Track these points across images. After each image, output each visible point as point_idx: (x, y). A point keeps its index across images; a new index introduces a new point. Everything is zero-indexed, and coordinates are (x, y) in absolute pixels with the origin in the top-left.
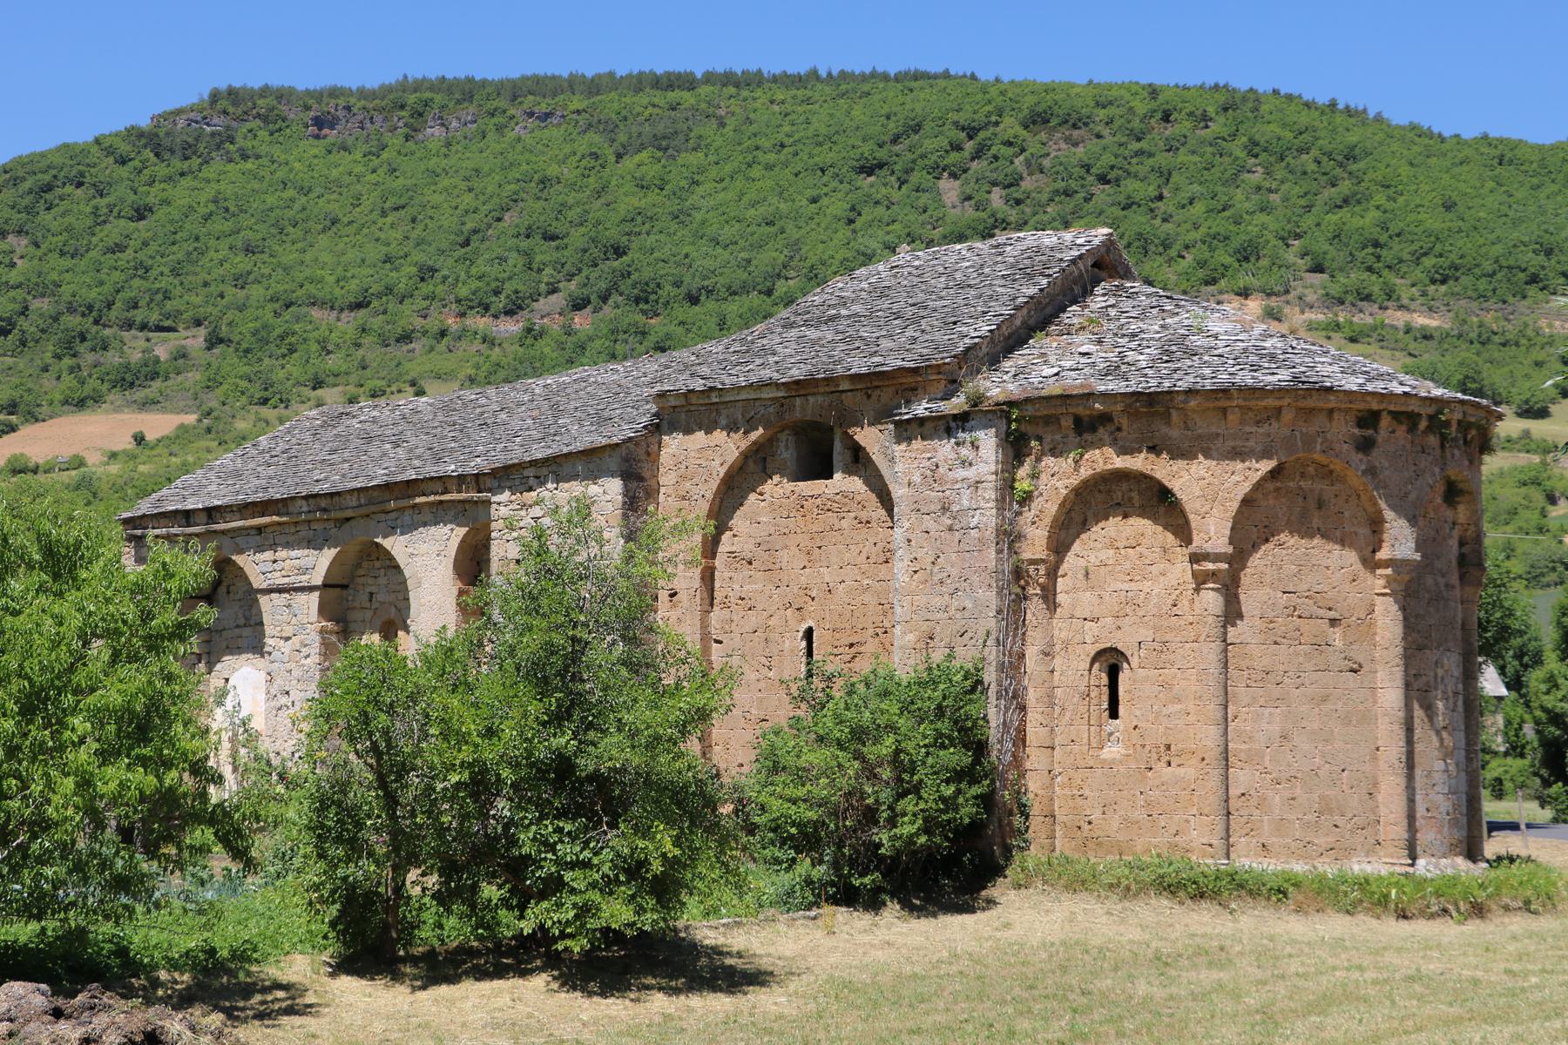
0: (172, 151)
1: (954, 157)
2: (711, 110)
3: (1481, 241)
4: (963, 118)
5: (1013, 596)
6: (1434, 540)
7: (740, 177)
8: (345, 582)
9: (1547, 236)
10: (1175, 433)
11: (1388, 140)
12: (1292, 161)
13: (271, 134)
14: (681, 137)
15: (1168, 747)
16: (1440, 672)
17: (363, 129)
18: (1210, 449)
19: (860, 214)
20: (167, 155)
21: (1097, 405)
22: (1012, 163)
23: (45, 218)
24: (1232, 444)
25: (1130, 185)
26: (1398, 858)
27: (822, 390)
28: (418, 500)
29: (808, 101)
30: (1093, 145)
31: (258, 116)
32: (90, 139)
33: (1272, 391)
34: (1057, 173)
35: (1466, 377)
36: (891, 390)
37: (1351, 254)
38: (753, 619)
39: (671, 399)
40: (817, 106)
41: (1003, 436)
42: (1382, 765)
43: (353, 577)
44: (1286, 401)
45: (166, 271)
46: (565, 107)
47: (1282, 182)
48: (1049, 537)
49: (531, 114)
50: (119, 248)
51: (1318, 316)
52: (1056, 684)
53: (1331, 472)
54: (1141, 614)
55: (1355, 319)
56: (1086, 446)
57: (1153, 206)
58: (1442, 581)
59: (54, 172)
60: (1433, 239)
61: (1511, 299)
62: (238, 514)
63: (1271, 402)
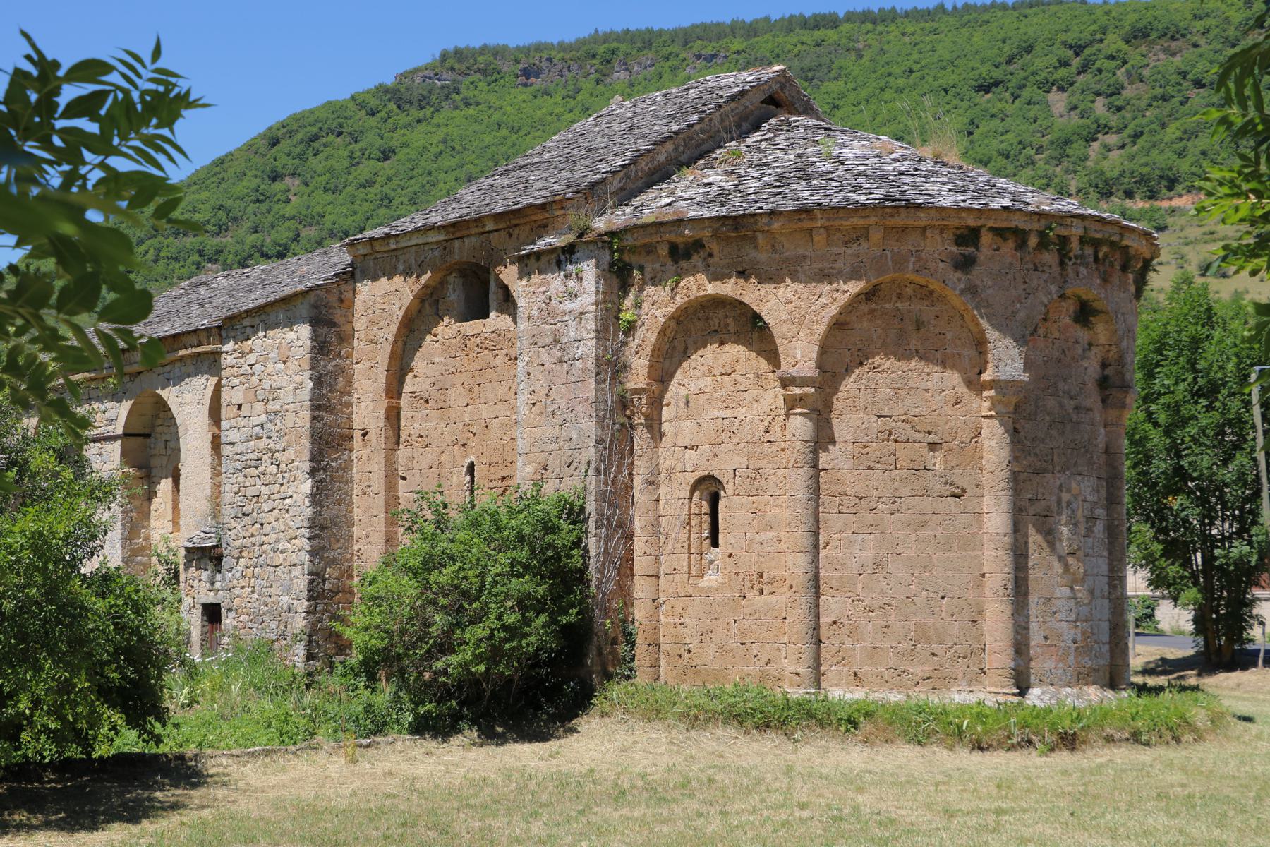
0: (411, 103)
1: (1062, 72)
2: (851, 44)
4: (1070, 38)
5: (618, 426)
6: (1059, 361)
7: (874, 100)
8: (146, 431)
10: (763, 257)
13: (489, 85)
14: (825, 68)
15: (761, 575)
16: (1065, 497)
17: (562, 76)
18: (798, 272)
19: (977, 127)
20: (406, 107)
21: (687, 232)
22: (1114, 74)
23: (314, 162)
24: (820, 265)
26: (1002, 687)
27: (473, 231)
28: (182, 353)
29: (935, 32)
30: (1191, 53)
31: (479, 70)
32: (348, 96)
33: (857, 209)
36: (527, 228)
38: (430, 456)
39: (360, 247)
40: (943, 35)
41: (606, 266)
42: (988, 592)
43: (153, 427)
44: (872, 220)
45: (405, 200)
46: (727, 49)
48: (651, 367)
49: (699, 57)
50: (369, 184)
52: (661, 514)
53: (931, 292)
54: (735, 440)
56: (681, 274)
58: (1070, 404)
59: (320, 125)
63: (856, 221)
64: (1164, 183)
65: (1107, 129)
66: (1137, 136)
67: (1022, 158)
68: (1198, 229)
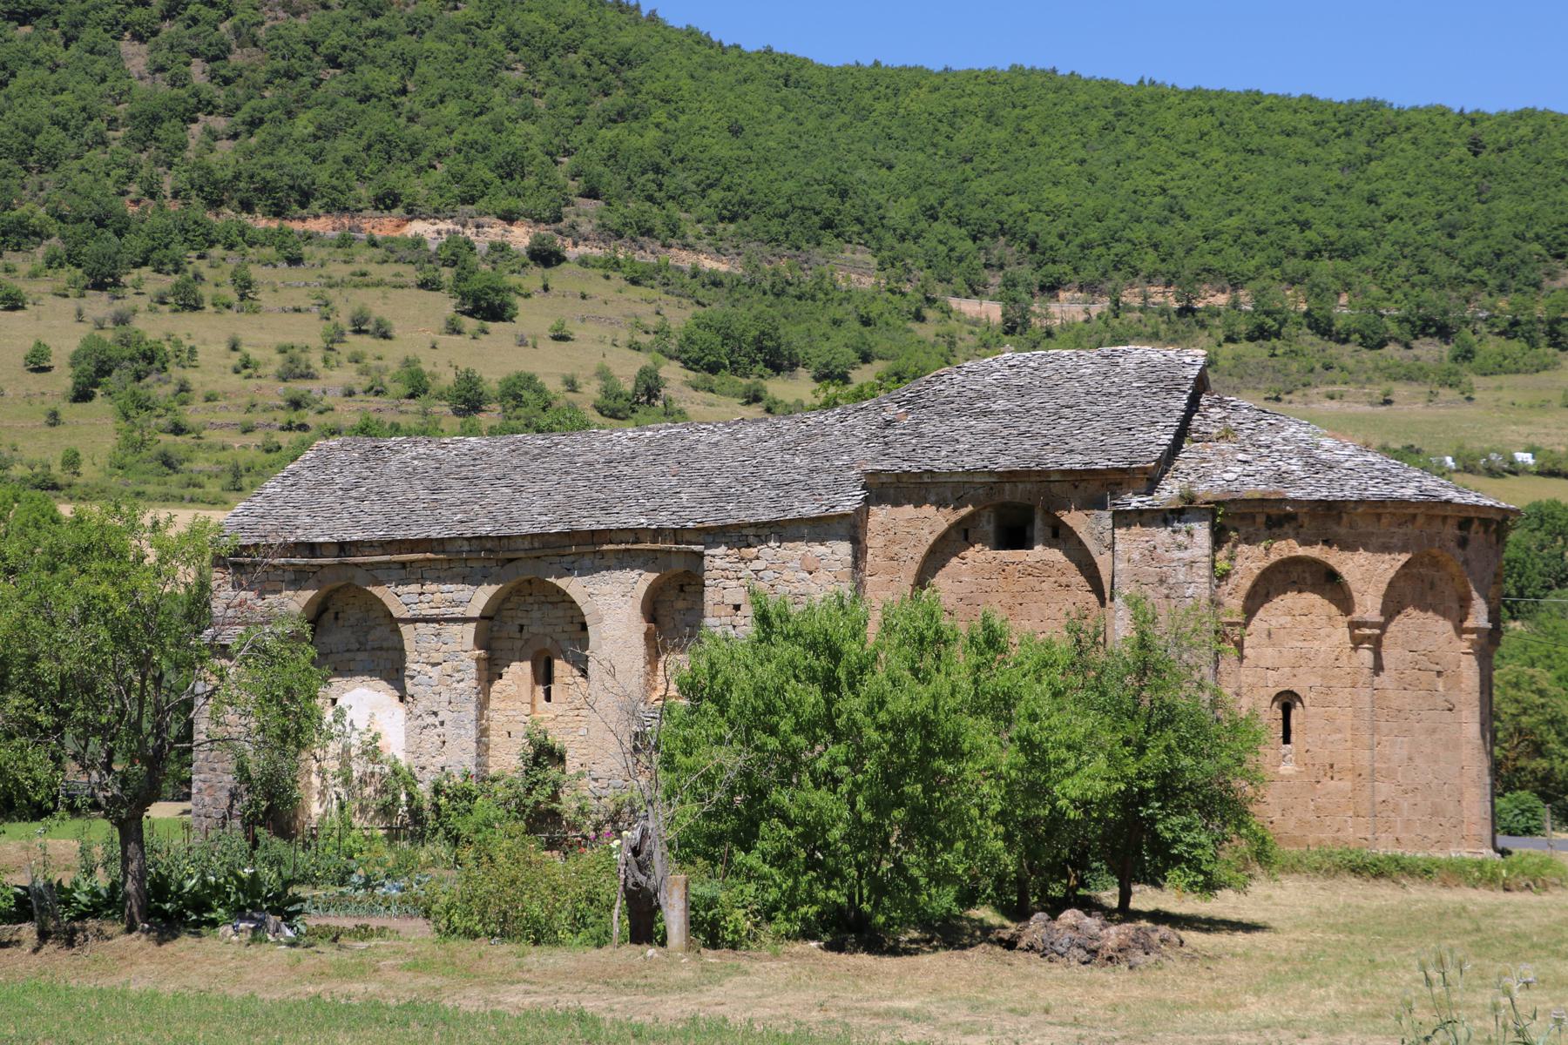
3: (773, 175)
9: (841, 175)
10: (1342, 530)
11: (666, 46)
12: (558, 61)
15: (1332, 766)
22: (217, 29)
25: (367, 73)
28: (605, 547)
34: (276, 48)
35: (763, 333)
37: (629, 179)
47: (548, 85)
51: (595, 251)
55: (636, 257)
57: (397, 101)
60: (720, 168)
61: (805, 246)
62: (380, 551)
63: (1411, 511)
64: (295, 195)
65: (210, 107)
66: (254, 124)
67: (88, 134)
68: (344, 266)
